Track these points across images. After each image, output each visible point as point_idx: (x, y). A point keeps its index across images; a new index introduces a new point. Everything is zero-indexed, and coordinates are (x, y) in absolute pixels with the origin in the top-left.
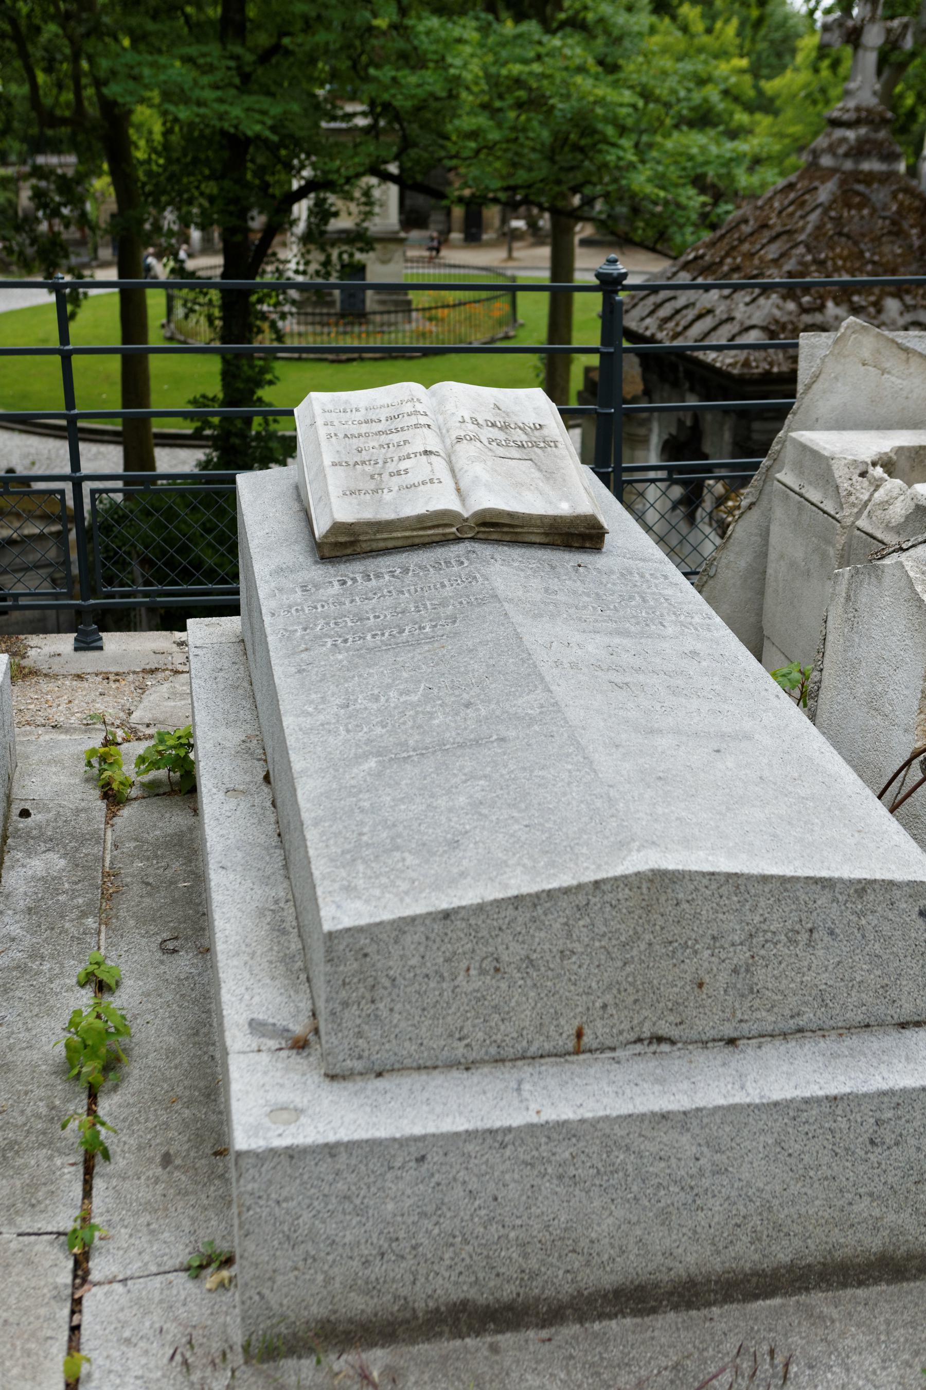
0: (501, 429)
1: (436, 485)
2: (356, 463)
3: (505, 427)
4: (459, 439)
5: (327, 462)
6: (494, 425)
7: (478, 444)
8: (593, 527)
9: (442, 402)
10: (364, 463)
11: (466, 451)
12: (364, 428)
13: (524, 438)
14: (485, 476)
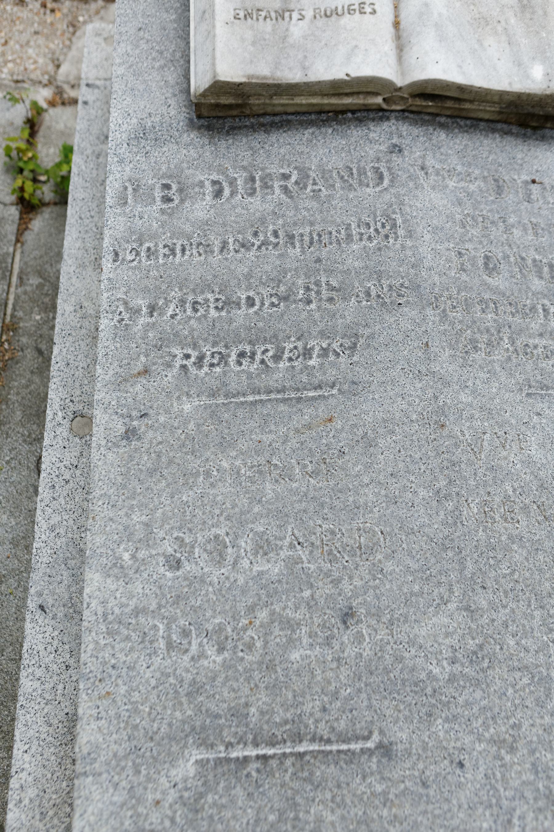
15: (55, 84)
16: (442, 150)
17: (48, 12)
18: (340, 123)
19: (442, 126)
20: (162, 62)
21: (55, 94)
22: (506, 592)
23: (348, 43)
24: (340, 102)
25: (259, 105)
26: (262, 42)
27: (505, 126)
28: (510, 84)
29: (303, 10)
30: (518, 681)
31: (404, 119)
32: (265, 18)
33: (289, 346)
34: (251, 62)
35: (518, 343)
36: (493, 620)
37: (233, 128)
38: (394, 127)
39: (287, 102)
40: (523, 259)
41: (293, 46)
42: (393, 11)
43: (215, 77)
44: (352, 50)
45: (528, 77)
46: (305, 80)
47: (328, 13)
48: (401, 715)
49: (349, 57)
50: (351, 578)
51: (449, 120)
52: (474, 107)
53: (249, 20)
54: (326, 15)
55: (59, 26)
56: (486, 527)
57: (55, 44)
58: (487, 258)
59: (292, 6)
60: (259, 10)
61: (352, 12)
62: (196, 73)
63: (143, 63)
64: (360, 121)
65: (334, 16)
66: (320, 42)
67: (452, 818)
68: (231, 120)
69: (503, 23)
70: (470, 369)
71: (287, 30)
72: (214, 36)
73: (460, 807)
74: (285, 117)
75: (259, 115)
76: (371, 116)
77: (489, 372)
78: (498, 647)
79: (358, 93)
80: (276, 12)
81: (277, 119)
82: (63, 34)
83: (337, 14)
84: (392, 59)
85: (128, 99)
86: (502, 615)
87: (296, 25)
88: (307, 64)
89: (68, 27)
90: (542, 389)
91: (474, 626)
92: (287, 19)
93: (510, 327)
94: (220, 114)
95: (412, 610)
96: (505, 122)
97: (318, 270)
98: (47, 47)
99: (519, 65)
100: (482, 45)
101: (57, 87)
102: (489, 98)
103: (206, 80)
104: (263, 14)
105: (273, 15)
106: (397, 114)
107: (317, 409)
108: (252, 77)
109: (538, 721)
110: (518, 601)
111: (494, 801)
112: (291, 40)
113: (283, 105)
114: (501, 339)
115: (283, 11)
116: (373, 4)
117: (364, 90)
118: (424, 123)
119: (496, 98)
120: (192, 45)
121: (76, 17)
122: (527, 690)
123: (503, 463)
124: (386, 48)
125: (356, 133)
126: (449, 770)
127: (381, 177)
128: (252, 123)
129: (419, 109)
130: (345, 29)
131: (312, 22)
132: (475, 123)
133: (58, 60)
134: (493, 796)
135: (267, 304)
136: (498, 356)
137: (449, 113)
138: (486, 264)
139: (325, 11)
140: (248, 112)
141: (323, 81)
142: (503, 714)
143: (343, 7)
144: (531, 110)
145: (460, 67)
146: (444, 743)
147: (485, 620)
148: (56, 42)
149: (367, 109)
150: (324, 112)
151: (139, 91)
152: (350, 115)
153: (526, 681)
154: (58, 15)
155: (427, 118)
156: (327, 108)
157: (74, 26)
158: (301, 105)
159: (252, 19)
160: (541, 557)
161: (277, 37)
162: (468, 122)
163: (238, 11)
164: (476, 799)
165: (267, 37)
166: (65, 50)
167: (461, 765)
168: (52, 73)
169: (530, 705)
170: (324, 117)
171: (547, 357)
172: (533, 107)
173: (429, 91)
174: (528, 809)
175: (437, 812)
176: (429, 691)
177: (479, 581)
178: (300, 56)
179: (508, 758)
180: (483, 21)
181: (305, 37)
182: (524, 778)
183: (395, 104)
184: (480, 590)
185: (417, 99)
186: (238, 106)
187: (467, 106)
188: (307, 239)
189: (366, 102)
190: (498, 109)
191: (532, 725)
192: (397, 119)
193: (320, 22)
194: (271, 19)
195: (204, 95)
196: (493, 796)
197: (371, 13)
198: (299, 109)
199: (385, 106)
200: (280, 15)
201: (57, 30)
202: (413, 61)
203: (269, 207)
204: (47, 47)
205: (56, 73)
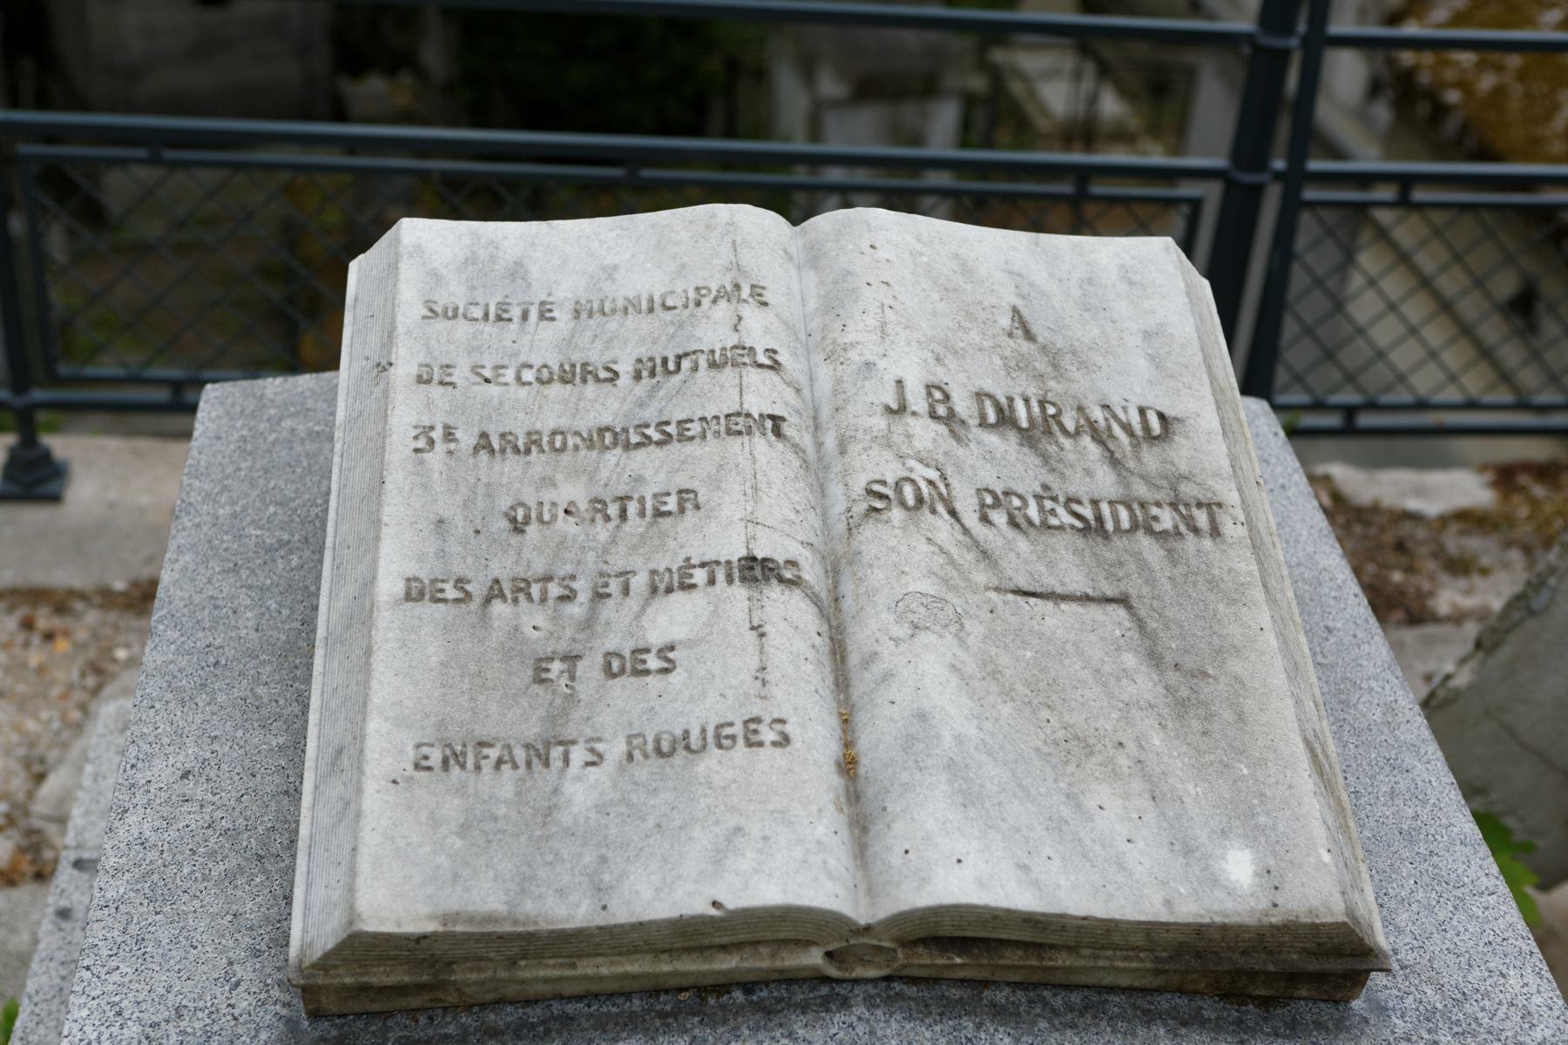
0: (1028, 437)
1: (768, 757)
2: (495, 592)
3: (1038, 433)
4: (878, 499)
5: (389, 586)
6: (1005, 419)
7: (942, 527)
8: (1338, 952)
9: (836, 301)
10: (522, 587)
11: (902, 558)
12: (554, 409)
13: (1105, 482)
14: (954, 711)
15: (23, 823)
17: (36, 639)
18: (708, 1020)
19: (1001, 1014)
20: (233, 861)
21: (21, 850)
23: (717, 822)
24: (705, 967)
25: (481, 983)
26: (487, 826)
27: (1181, 1001)
28: (1168, 903)
29: (599, 740)
31: (891, 1000)
32: (499, 762)
34: (456, 877)
38: (861, 1029)
39: (557, 973)
41: (569, 833)
42: (838, 732)
43: (351, 923)
44: (729, 840)
45: (1215, 881)
46: (602, 920)
47: (665, 746)
49: (719, 859)
52: (1081, 963)
53: (455, 770)
54: (659, 752)
55: (60, 675)
57: (42, 722)
59: (570, 732)
60: (482, 744)
61: (726, 743)
62: (307, 907)
63: (180, 864)
64: (767, 1011)
65: (681, 752)
66: (644, 820)
68: (404, 1020)
69: (1131, 747)
71: (556, 791)
72: (358, 815)
74: (556, 1008)
75: (483, 1006)
76: (799, 997)
80: (528, 746)
81: (535, 1014)
82: (64, 696)
83: (688, 748)
84: (839, 856)
85: (124, 969)
87: (579, 778)
88: (607, 877)
89: (83, 675)
92: (557, 763)
96: (1181, 991)
98: (17, 729)
99: (1188, 852)
100: (1079, 806)
101: (30, 832)
102: (1117, 939)
103: (329, 928)
104: (494, 753)
105: (520, 755)
106: (870, 988)
108: (457, 917)
112: (565, 818)
113: (546, 981)
115: (548, 745)
116: (782, 721)
117: (769, 935)
118: (949, 1009)
119: (1138, 939)
120: (304, 831)
121: (107, 653)
124: (821, 830)
128: (464, 1028)
129: (933, 973)
130: (710, 785)
131: (621, 768)
132: (1095, 998)
133: (42, 760)
137: (1017, 978)
139: (658, 741)
140: (452, 998)
141: (651, 922)
143: (704, 731)
144: (1242, 962)
145: (1024, 868)
148: (44, 715)
149: (790, 979)
150: (667, 991)
151: (158, 943)
152: (738, 995)
154: (62, 645)
155: (956, 993)
156: (673, 983)
157: (98, 671)
158: (601, 978)
159: (463, 766)
161: (528, 811)
162: (1075, 998)
163: (425, 750)
165: (502, 810)
166: (66, 735)
168: (21, 796)
170: (666, 1003)
172: (1244, 953)
173: (947, 930)
180: (1075, 747)
181: (603, 809)
183: (863, 962)
185: (921, 950)
186: (420, 988)
187: (1062, 960)
189: (778, 964)
190: (1148, 965)
192: (870, 1002)
193: (643, 771)
194: (515, 767)
195: (326, 963)
197: (774, 744)
198: (594, 988)
199: (833, 972)
200: (539, 754)
201: (53, 683)
202: (896, 859)
204: (17, 729)
205: (30, 795)
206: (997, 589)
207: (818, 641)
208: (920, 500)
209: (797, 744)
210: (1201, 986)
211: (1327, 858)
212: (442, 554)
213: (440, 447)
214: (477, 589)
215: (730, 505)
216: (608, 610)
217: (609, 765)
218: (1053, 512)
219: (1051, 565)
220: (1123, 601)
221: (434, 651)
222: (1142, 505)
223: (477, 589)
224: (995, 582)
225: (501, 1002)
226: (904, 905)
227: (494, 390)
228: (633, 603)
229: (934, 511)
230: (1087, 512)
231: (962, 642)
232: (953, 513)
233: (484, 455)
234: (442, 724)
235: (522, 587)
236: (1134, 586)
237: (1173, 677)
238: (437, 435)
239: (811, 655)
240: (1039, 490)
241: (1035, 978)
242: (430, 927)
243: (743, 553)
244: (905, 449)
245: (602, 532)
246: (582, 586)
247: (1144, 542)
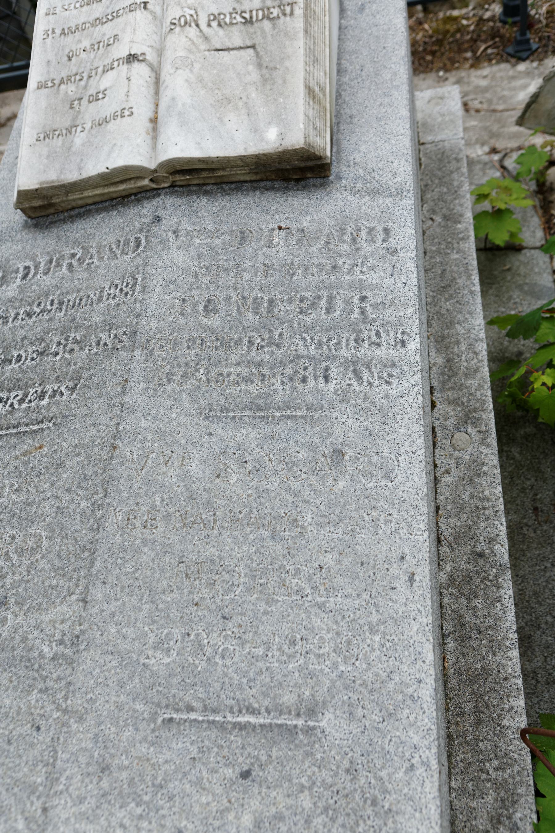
2: (62, 82)
16: (199, 214)
19: (206, 193)
22: (123, 588)
24: (117, 189)
28: (245, 149)
30: (107, 663)
33: (32, 390)
34: (45, 171)
35: (213, 373)
36: (103, 611)
37: (51, 223)
40: (244, 298)
41: (74, 153)
45: (263, 140)
46: (80, 177)
48: (11, 685)
50: (13, 574)
51: (215, 187)
52: (226, 173)
56: (124, 532)
58: (209, 301)
59: (78, 122)
67: (19, 772)
69: (244, 99)
70: (158, 399)
73: (27, 763)
77: (175, 400)
78: (100, 633)
79: (130, 179)
86: (112, 607)
90: (222, 412)
91: (84, 614)
92: (73, 133)
93: (209, 359)
94: (43, 214)
95: (46, 600)
96: (267, 180)
97: (71, 328)
99: (256, 131)
104: (57, 133)
105: (64, 132)
107: (34, 439)
109: (114, 699)
110: (132, 596)
111: (51, 760)
112: (73, 149)
114: (197, 370)
122: (113, 672)
123: (160, 478)
125: (132, 211)
126: (29, 732)
127: (138, 246)
134: (52, 757)
135: (29, 358)
136: (189, 386)
138: (206, 307)
142: (84, 689)
144: (278, 166)
146: (33, 710)
147: (95, 610)
153: (114, 663)
156: (114, 195)
160: (168, 560)
162: (233, 186)
164: (40, 758)
165: (58, 150)
167: (38, 729)
169: (111, 685)
171: (238, 383)
174: (78, 772)
175: (11, 765)
176: (36, 667)
177: (102, 577)
178: (78, 160)
179: (75, 726)
181: (83, 145)
182: (83, 745)
184: (100, 585)
187: (220, 173)
188: (71, 303)
191: (107, 701)
196: (52, 757)
199: (154, 186)
203: (54, 282)
206: (209, 50)
207: (149, 79)
208: (186, 23)
209: (135, 115)
210: (273, 177)
211: (302, 126)
212: (48, 72)
213: (50, 37)
214: (57, 82)
215: (126, 38)
216: (91, 81)
217: (86, 131)
218: (235, 18)
219: (230, 38)
220: (253, 47)
221: (43, 103)
222: (268, 9)
223: (57, 82)
224: (208, 48)
225: (73, 208)
226: (160, 161)
227: (68, 12)
228: (98, 77)
229: (190, 26)
230: (247, 16)
231: (191, 71)
232: (197, 25)
233: (63, 36)
234: (44, 126)
235: (69, 79)
236: (258, 40)
237: (264, 71)
238: (50, 32)
239: (145, 84)
240: (231, 10)
241: (219, 181)
242: (37, 186)
243: (128, 53)
244: (184, 5)
245: (92, 55)
246: (85, 75)
247: (266, 23)
